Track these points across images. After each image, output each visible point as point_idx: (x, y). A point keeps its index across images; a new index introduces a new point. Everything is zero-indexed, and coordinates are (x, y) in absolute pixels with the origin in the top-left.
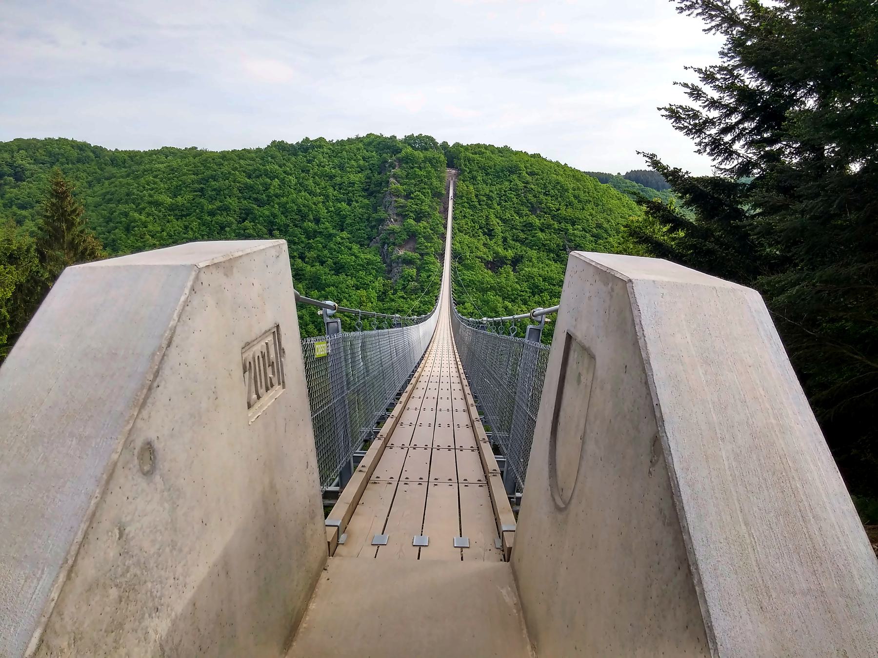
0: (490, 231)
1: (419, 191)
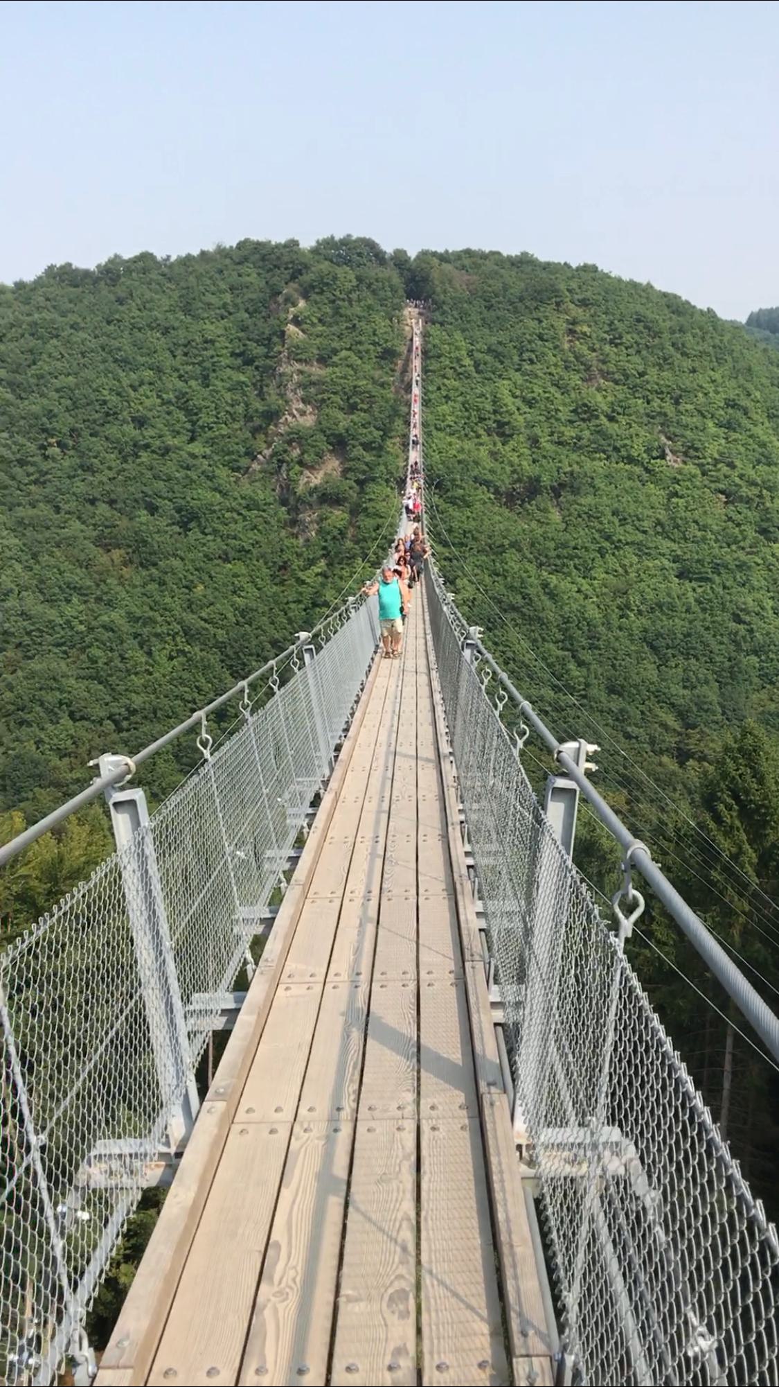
0: (501, 425)
1: (350, 349)
